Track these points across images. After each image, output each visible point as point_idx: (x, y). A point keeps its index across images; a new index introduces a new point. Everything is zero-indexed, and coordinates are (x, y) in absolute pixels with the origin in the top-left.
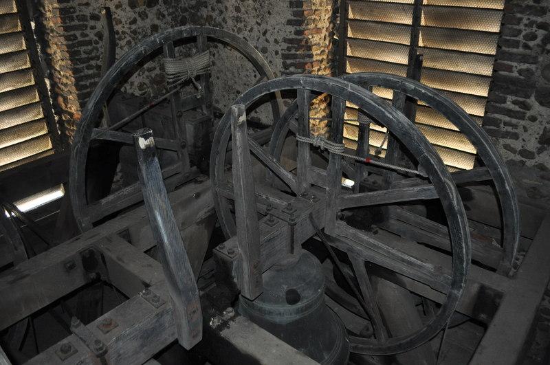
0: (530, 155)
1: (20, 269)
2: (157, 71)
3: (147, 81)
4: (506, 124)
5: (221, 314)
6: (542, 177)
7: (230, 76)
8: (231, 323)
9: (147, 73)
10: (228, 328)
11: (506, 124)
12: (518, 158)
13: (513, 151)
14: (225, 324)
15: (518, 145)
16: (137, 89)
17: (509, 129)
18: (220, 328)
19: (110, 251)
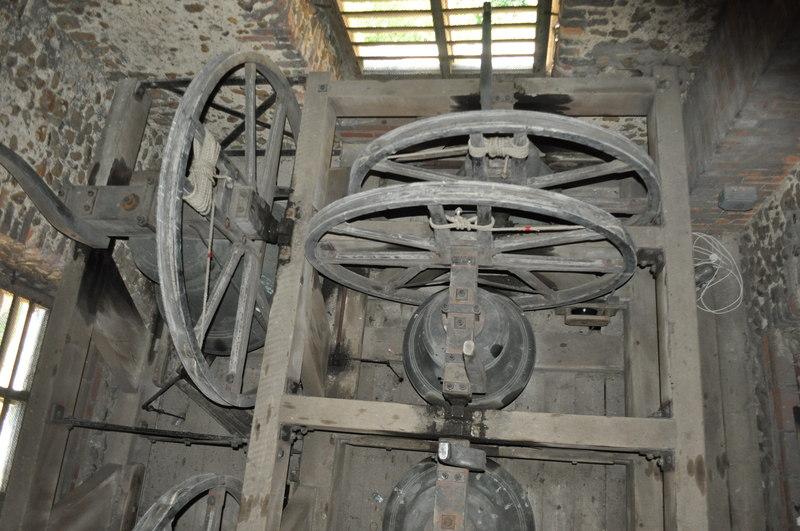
0: (624, 34)
1: (251, 496)
2: (39, 93)
3: (41, 122)
4: (591, 13)
5: (472, 421)
6: (638, 49)
7: (147, 35)
8: (485, 422)
9: (32, 112)
10: (487, 428)
11: (591, 13)
12: (609, 38)
13: (603, 34)
14: (483, 428)
15: (609, 28)
16: (40, 143)
17: (596, 17)
18: (482, 433)
19: (307, 419)
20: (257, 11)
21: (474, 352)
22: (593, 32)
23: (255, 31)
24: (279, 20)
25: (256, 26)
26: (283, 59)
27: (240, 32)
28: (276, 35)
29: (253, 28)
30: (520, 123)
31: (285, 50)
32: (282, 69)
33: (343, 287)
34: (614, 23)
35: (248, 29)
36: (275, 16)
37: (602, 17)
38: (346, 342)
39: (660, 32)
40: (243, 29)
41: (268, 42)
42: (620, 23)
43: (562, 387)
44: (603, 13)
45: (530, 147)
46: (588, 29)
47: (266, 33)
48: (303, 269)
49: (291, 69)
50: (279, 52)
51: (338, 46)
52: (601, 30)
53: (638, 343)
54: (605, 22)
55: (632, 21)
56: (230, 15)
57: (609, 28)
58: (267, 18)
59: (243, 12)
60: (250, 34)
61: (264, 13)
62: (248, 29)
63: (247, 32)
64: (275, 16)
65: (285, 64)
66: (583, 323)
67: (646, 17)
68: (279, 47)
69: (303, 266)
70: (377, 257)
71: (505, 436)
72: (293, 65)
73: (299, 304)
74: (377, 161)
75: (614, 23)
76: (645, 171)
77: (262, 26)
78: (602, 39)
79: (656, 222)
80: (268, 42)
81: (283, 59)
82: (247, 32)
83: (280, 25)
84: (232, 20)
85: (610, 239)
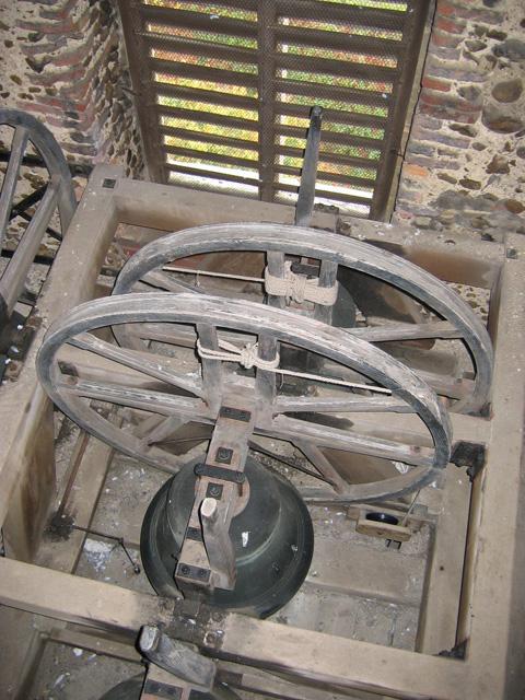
4: (440, 152)
13: (452, 181)
17: (447, 158)
20: (49, 74)
21: (214, 514)
22: (443, 177)
23: (41, 99)
24: (73, 89)
25: (43, 93)
26: (69, 141)
27: (24, 96)
28: (64, 109)
29: (39, 94)
30: (330, 248)
31: (73, 130)
32: (65, 153)
33: (87, 432)
34: (466, 170)
35: (33, 94)
36: (68, 84)
37: (454, 160)
38: (73, 506)
39: (518, 191)
40: (28, 93)
41: (54, 116)
42: (474, 170)
43: (341, 615)
44: (455, 155)
45: (339, 288)
46: (435, 171)
47: (53, 102)
48: (32, 396)
49: (77, 156)
50: (66, 130)
51: (142, 146)
52: (450, 175)
53: (442, 569)
54: (456, 166)
55: (488, 172)
56: (14, 73)
57: (459, 175)
58: (58, 85)
59: (31, 71)
60: (35, 102)
61: (57, 78)
62: (33, 94)
63: (31, 98)
64: (68, 84)
65: (71, 148)
66: (380, 532)
67: (505, 170)
68: (67, 124)
69: (35, 389)
70: (129, 393)
71: (246, 651)
72: (80, 150)
73: (16, 439)
74: (149, 269)
75: (466, 170)
76: (475, 338)
77: (50, 92)
78: (451, 187)
79: (484, 412)
80: (54, 116)
81: (69, 141)
82: (31, 98)
83: (72, 96)
84: (16, 79)
85: (423, 412)
